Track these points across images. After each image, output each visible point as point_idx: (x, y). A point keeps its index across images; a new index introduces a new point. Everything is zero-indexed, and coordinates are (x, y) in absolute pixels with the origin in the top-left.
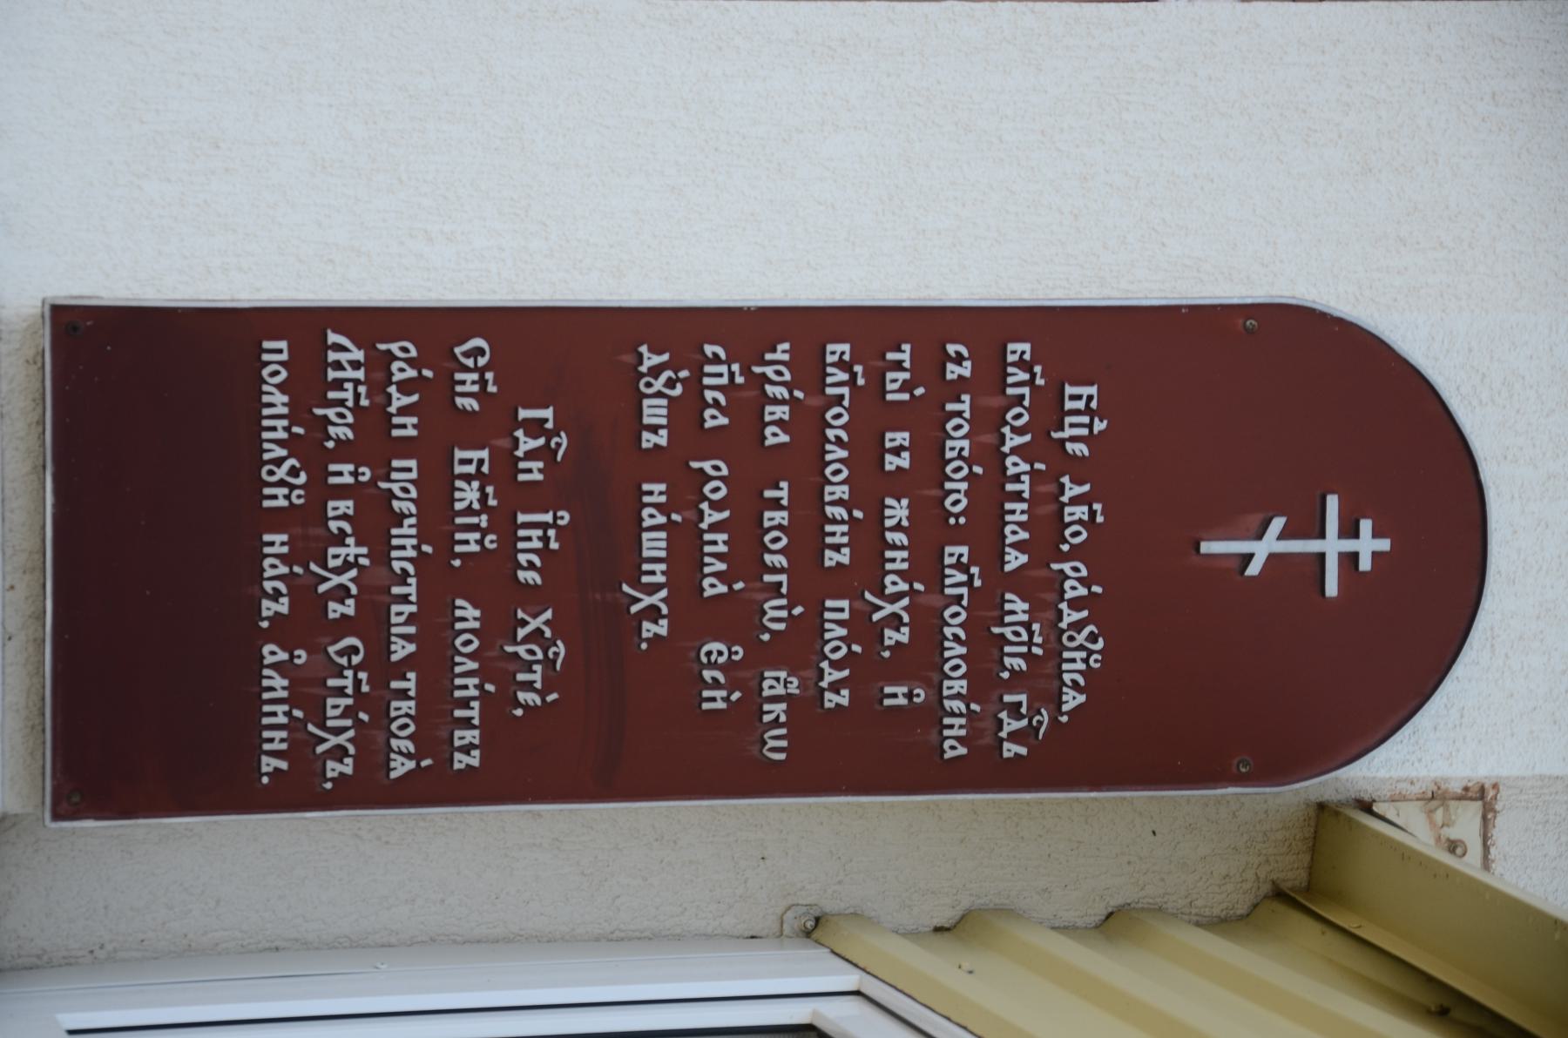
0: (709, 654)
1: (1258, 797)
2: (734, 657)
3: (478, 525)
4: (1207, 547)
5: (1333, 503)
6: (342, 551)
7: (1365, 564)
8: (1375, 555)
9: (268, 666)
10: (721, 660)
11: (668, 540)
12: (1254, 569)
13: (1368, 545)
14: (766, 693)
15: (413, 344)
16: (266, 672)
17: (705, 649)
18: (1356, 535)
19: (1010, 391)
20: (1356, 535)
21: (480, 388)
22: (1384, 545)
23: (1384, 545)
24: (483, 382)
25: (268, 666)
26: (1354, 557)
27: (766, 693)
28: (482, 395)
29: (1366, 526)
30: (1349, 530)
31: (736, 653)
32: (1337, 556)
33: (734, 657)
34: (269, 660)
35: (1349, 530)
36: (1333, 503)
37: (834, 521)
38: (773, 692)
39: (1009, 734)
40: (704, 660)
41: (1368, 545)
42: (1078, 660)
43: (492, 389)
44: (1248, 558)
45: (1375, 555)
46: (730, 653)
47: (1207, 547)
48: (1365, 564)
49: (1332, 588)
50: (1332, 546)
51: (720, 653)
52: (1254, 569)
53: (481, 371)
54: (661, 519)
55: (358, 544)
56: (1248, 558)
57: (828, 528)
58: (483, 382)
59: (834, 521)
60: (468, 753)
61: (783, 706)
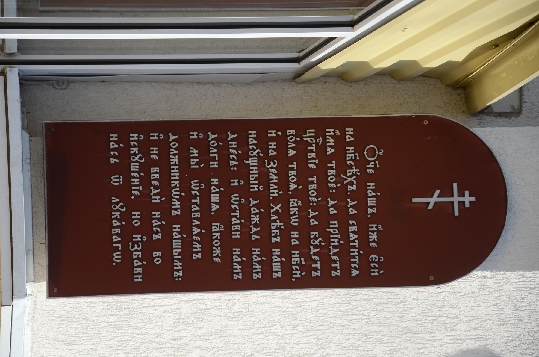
0: (372, 258)
1: (32, 186)
2: (380, 260)
3: (139, 189)
4: (414, 200)
5: (455, 185)
6: (276, 224)
7: (467, 205)
8: (470, 202)
9: (235, 262)
10: (376, 260)
11: (219, 196)
12: (430, 207)
13: (468, 199)
14: (213, 230)
15: (116, 152)
16: (234, 264)
17: (370, 257)
18: (464, 196)
19: (211, 155)
20: (464, 196)
21: (374, 166)
22: (473, 199)
23: (473, 199)
24: (375, 165)
25: (235, 262)
26: (464, 202)
27: (213, 230)
28: (375, 168)
29: (467, 193)
30: (461, 194)
31: (381, 259)
32: (453, 201)
33: (380, 260)
34: (235, 260)
35: (461, 194)
36: (455, 185)
37: (134, 178)
38: (216, 230)
39: (313, 253)
40: (371, 260)
41: (468, 199)
42: (157, 199)
43: (378, 166)
44: (428, 203)
45: (470, 202)
46: (379, 259)
47: (414, 200)
48: (467, 205)
49: (457, 213)
50: (456, 199)
51: (376, 258)
52: (430, 207)
53: (374, 161)
54: (217, 190)
55: (280, 222)
56: (428, 203)
57: (133, 180)
58: (375, 165)
59: (134, 178)
60: (238, 275)
61: (219, 234)
